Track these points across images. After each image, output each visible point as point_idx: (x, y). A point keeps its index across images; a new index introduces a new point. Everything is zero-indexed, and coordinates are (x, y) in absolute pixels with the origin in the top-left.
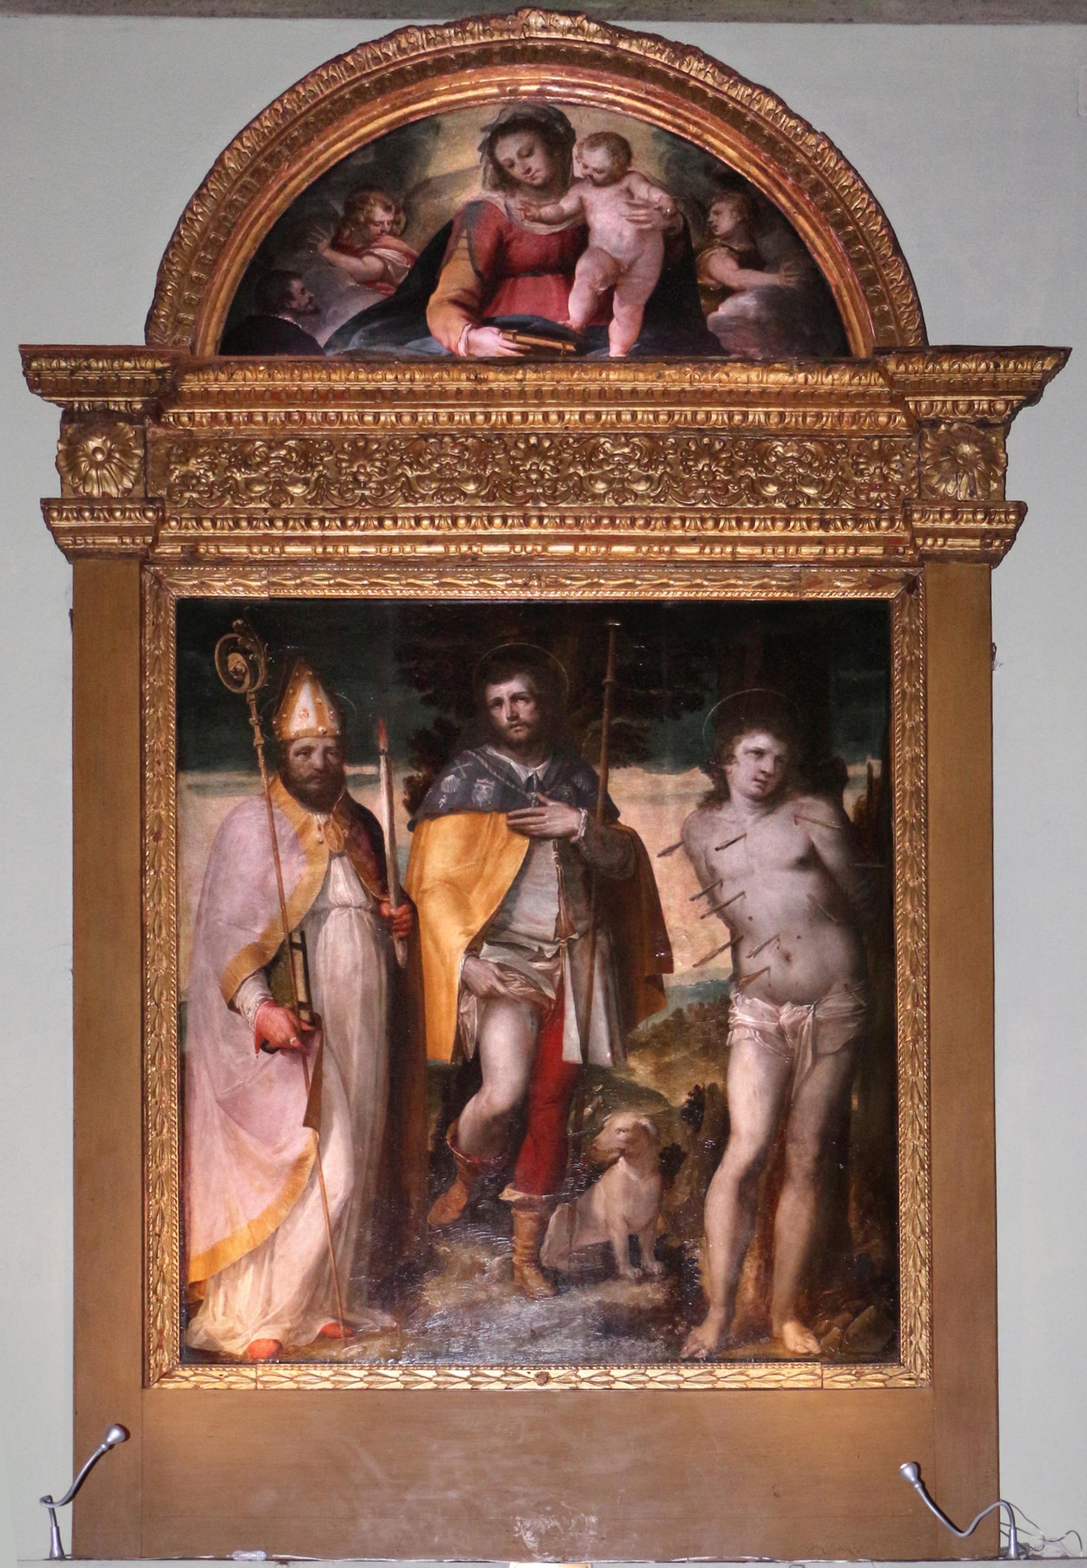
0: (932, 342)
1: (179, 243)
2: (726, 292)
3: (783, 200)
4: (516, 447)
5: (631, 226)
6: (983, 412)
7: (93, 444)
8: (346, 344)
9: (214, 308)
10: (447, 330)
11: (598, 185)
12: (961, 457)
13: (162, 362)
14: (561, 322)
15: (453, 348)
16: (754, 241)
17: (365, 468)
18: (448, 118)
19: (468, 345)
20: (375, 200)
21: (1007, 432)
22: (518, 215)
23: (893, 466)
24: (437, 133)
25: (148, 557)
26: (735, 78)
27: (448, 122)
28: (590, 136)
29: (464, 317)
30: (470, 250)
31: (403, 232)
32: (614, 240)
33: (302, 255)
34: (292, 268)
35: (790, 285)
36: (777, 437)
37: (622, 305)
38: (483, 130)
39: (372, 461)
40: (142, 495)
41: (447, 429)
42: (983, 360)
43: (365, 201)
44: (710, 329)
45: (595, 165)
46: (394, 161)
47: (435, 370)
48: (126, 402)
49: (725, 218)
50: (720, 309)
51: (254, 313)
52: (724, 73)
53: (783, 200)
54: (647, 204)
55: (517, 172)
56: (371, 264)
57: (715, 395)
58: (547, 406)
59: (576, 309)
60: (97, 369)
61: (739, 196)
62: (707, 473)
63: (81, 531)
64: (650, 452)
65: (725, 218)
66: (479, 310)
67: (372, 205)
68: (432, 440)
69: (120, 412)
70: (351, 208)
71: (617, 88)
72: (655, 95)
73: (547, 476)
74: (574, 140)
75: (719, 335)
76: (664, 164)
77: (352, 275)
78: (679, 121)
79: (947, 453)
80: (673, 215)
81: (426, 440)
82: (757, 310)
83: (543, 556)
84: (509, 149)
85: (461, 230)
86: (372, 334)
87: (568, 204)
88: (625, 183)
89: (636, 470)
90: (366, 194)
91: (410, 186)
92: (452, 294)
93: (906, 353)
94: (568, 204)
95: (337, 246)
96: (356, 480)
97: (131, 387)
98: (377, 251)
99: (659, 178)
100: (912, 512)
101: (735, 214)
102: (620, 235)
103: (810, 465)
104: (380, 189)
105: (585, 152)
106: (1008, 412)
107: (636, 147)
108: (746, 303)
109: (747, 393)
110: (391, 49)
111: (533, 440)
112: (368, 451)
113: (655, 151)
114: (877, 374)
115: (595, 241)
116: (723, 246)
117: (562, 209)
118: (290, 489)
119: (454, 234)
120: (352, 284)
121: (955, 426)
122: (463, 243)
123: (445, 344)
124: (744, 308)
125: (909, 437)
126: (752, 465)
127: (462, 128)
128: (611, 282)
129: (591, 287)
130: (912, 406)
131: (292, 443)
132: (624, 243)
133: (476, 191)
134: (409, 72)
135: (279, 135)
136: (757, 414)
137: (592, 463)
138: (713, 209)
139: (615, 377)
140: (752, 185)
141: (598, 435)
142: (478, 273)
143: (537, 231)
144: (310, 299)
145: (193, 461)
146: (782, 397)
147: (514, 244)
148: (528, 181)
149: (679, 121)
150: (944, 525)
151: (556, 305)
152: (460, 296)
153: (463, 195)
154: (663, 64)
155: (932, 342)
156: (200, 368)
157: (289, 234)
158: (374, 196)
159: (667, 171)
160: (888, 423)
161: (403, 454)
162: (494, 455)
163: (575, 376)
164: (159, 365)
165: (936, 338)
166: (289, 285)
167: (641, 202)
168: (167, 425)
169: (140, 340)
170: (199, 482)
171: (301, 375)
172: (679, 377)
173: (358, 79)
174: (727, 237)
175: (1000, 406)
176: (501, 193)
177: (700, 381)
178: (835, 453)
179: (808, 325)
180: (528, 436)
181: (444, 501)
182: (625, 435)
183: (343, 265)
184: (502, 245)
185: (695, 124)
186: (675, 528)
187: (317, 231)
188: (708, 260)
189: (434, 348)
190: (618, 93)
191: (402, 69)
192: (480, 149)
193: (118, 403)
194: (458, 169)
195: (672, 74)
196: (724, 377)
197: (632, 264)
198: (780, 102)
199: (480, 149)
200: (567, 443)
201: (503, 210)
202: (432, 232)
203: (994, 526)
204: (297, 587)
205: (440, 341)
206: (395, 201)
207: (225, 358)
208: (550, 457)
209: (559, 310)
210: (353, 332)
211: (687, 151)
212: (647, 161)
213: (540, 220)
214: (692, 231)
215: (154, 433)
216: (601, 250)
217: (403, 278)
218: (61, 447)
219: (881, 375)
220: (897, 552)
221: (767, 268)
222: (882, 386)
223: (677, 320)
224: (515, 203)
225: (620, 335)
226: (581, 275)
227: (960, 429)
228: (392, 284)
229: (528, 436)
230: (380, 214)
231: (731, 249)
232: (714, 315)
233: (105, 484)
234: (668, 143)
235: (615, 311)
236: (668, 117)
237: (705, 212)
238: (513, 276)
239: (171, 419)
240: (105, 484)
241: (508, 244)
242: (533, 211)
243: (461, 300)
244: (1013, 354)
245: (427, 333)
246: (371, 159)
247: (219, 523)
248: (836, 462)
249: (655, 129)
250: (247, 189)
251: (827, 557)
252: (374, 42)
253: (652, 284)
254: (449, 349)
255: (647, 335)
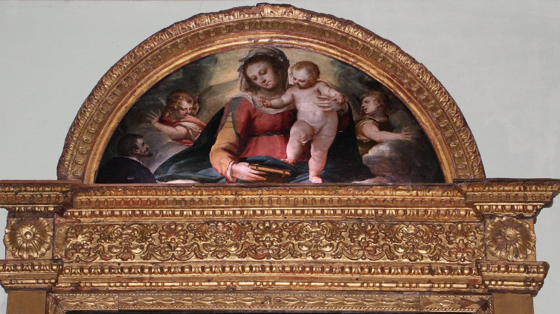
0: (488, 176)
1: (78, 124)
2: (373, 143)
3: (402, 95)
4: (258, 228)
5: (320, 109)
6: (520, 211)
7: (26, 230)
8: (166, 172)
9: (95, 154)
10: (220, 164)
11: (301, 88)
12: (508, 237)
13: (66, 188)
14: (282, 160)
15: (224, 174)
16: (387, 117)
17: (175, 240)
18: (222, 55)
19: (232, 172)
20: (183, 97)
21: (535, 222)
22: (259, 104)
23: (470, 238)
24: (216, 63)
25: (52, 289)
26: (373, 36)
27: (221, 57)
28: (297, 63)
29: (230, 157)
30: (233, 122)
31: (197, 113)
32: (311, 116)
33: (144, 125)
34: (137, 133)
35: (407, 139)
36: (403, 222)
37: (315, 151)
38: (240, 61)
39: (178, 235)
40: (50, 257)
41: (220, 219)
42: (517, 185)
43: (177, 98)
44: (364, 163)
45: (300, 78)
46: (192, 78)
47: (214, 190)
48: (45, 207)
49: (371, 104)
50: (370, 152)
51: (116, 156)
52: (368, 34)
53: (402, 95)
54: (328, 98)
55: (258, 82)
56: (180, 130)
57: (367, 202)
58: (275, 206)
59: (291, 153)
60: (30, 191)
61: (378, 93)
62: (364, 243)
63: (15, 278)
64: (332, 231)
65: (371, 104)
66: (237, 154)
67: (181, 100)
68: (212, 224)
69: (41, 212)
70: (170, 101)
71: (311, 40)
72: (331, 43)
73: (275, 244)
74: (289, 66)
75: (369, 166)
76: (337, 78)
77: (170, 136)
78: (344, 56)
79: (500, 234)
80: (342, 104)
81: (209, 224)
82: (391, 152)
83: (273, 288)
84: (254, 70)
85: (229, 112)
86: (180, 166)
87: (286, 98)
88: (317, 86)
89: (324, 240)
90: (178, 94)
91: (201, 90)
92: (223, 146)
93: (472, 182)
94: (286, 98)
95: (162, 121)
96: (170, 246)
97: (49, 200)
98: (183, 124)
99: (334, 84)
100: (482, 266)
101: (376, 102)
102: (314, 114)
103: (422, 237)
104: (185, 91)
105: (294, 71)
106: (535, 211)
107: (321, 69)
108: (383, 149)
109: (385, 200)
110: (192, 24)
111: (267, 225)
112: (177, 231)
113: (332, 70)
114: (457, 191)
115: (300, 117)
116: (371, 119)
117: (283, 101)
118: (133, 251)
119: (225, 114)
120: (170, 141)
121: (504, 218)
122: (230, 119)
123: (220, 172)
124: (383, 151)
125: (478, 222)
126: (389, 238)
127: (229, 60)
128: (309, 139)
129: (298, 141)
130: (478, 208)
131: (135, 226)
132: (316, 118)
133: (236, 92)
134: (201, 34)
135: (133, 67)
136: (390, 211)
137: (300, 237)
138: (364, 100)
139: (310, 194)
140: (386, 88)
141: (303, 221)
142: (237, 134)
143: (269, 113)
144: (147, 149)
145: (80, 236)
146: (404, 203)
147: (257, 119)
148: (264, 86)
149: (344, 56)
150: (501, 274)
151: (280, 151)
152: (227, 146)
153: (230, 95)
154: (335, 29)
155: (487, 177)
156: (86, 190)
157: (136, 115)
158: (182, 95)
159: (339, 80)
160: (466, 215)
161: (196, 232)
162: (246, 232)
163: (289, 193)
164: (64, 189)
165: (490, 174)
166: (136, 142)
167: (326, 97)
168: (66, 217)
169: (53, 177)
170: (83, 248)
171: (141, 193)
172: (345, 194)
173: (174, 39)
174: (372, 114)
175: (530, 208)
176: (250, 93)
177: (358, 195)
178: (436, 231)
179: (419, 164)
180: (265, 222)
181: (218, 258)
182: (318, 221)
183: (166, 131)
184: (250, 120)
185: (353, 57)
186: (347, 273)
187: (151, 113)
188: (362, 126)
189: (213, 174)
190: (312, 42)
191: (198, 33)
192: (238, 71)
193: (40, 208)
194: (227, 81)
195: (339, 33)
196: (371, 192)
197: (320, 129)
198: (398, 48)
199: (238, 71)
200: (286, 226)
201: (251, 102)
202: (213, 113)
203: (531, 275)
204: (134, 305)
205: (217, 170)
206: (193, 97)
207: (100, 185)
208: (276, 233)
209: (282, 153)
210: (169, 166)
211: (349, 70)
212: (328, 74)
213: (271, 107)
214: (353, 111)
215: (59, 221)
216: (304, 122)
217: (197, 137)
218: (7, 231)
219: (459, 191)
220: (475, 287)
221: (394, 130)
222: (460, 197)
223: (346, 160)
224: (257, 98)
225: (314, 164)
226: (293, 135)
227: (508, 220)
228: (191, 140)
229: (265, 222)
230: (185, 105)
231: (375, 121)
232: (366, 156)
233: (30, 250)
234: (339, 66)
235: (312, 154)
236: (339, 54)
237: (360, 101)
238: (255, 136)
239: (69, 214)
240: (30, 250)
241: (254, 119)
242: (268, 102)
243: (228, 148)
244: (534, 182)
245: (210, 166)
246: (181, 76)
247: (93, 270)
248: (437, 236)
249: (332, 59)
250: (115, 94)
251: (434, 290)
252: (183, 21)
253: (332, 139)
254: (222, 174)
255: (329, 166)
